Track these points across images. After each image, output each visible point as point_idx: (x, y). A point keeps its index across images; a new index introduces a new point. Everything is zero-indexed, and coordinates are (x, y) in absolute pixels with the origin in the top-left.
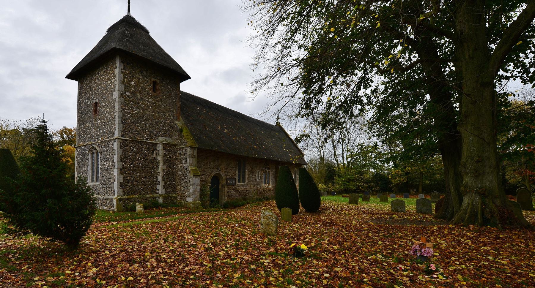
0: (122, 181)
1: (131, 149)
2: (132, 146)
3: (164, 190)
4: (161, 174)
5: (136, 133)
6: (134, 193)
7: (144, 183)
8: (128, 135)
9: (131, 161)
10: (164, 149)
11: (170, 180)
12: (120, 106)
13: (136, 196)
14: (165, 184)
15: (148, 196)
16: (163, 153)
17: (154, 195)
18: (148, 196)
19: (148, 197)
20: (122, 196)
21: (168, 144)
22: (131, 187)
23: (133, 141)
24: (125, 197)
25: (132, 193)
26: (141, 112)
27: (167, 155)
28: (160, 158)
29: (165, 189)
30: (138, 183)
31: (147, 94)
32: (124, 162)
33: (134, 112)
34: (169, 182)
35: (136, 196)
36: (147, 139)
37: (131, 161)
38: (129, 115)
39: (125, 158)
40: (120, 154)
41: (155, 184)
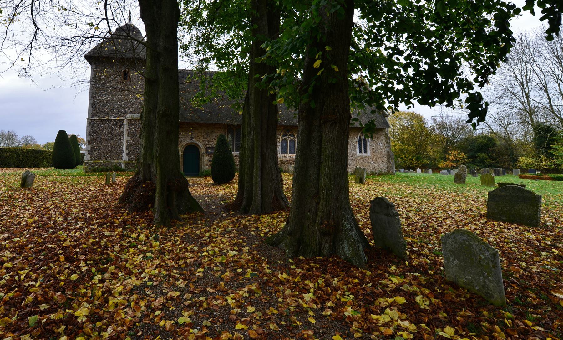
3: (127, 157)
4: (125, 144)
10: (129, 124)
13: (101, 161)
14: (129, 152)
15: (113, 161)
17: (119, 161)
18: (113, 161)
21: (133, 119)
23: (101, 120)
24: (91, 161)
27: (132, 129)
28: (125, 131)
32: (92, 135)
33: (103, 98)
35: (101, 161)
36: (114, 117)
39: (93, 133)
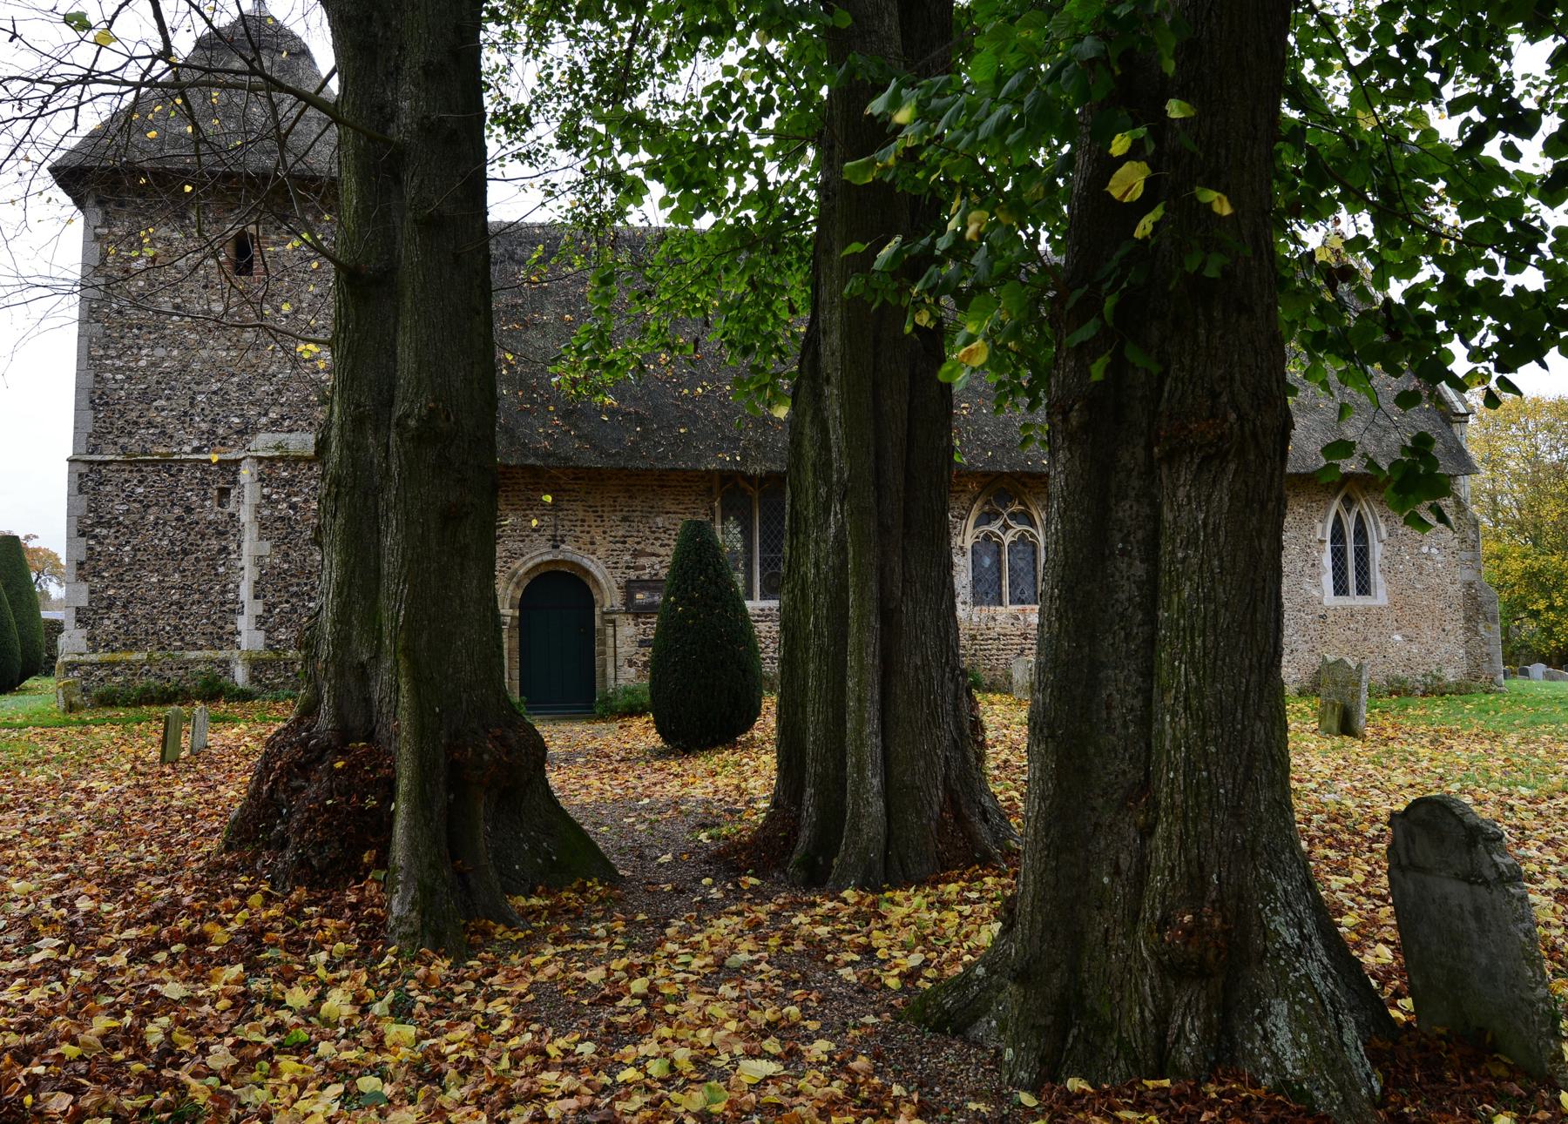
0: (84, 603)
1: (123, 491)
2: (127, 481)
3: (261, 635)
5: (153, 434)
6: (135, 643)
7: (181, 608)
8: (115, 444)
9: (124, 534)
11: (295, 594)
12: (85, 352)
16: (258, 495)
17: (221, 655)
19: (190, 661)
20: (82, 654)
21: (281, 459)
22: (121, 621)
25: (124, 645)
26: (173, 358)
27: (277, 502)
29: (266, 631)
30: (154, 607)
31: (205, 287)
32: (95, 537)
33: (143, 363)
34: (287, 602)
36: (198, 450)
37: (124, 534)
38: (119, 377)
40: (79, 513)
41: (233, 611)
